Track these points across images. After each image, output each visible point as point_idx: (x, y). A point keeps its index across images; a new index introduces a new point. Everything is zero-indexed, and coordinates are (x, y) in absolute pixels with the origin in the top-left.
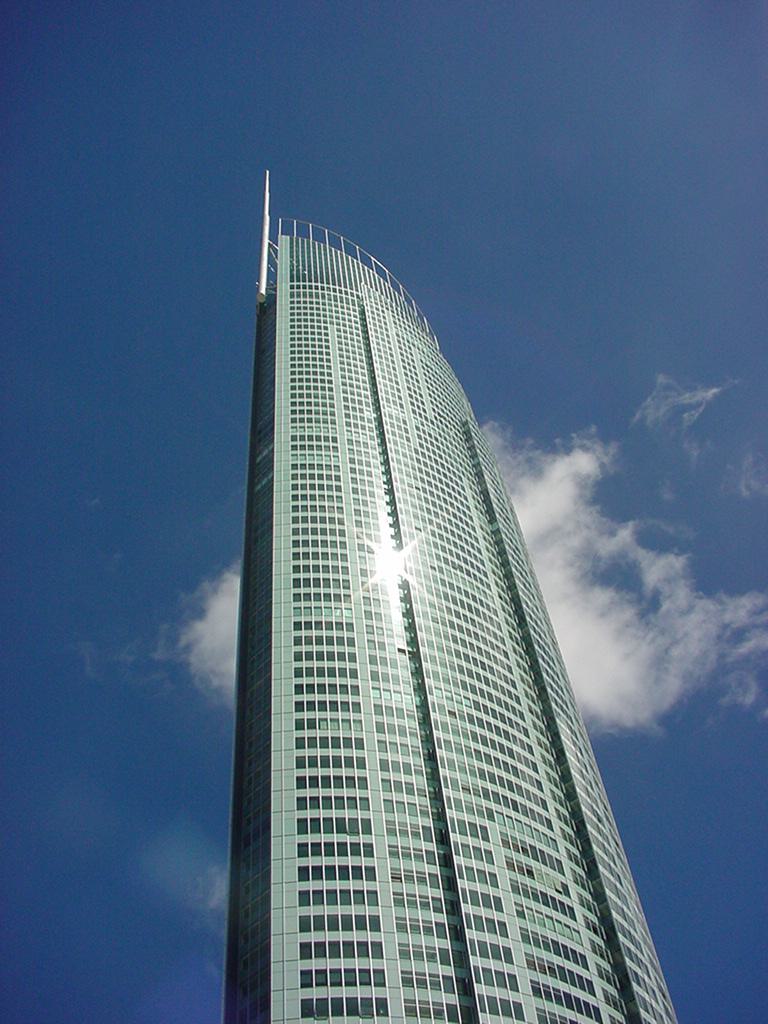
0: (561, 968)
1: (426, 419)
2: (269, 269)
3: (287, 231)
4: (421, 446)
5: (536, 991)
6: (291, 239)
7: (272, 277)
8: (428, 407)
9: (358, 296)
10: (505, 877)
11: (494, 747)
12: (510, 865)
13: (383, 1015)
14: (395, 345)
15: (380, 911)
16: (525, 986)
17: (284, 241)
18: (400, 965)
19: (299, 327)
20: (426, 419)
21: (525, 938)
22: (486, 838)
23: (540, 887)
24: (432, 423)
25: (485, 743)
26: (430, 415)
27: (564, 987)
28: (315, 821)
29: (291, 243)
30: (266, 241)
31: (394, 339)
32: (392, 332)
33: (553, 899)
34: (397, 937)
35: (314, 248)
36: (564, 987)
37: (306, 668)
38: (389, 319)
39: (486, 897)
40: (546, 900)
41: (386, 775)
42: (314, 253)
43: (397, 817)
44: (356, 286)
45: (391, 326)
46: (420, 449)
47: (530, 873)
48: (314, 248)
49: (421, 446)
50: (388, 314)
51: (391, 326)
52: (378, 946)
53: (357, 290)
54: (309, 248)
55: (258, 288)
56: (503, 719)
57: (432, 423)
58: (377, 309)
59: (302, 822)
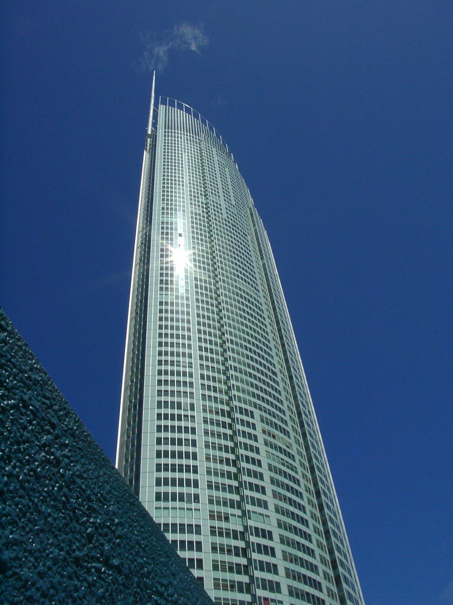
0: (287, 485)
1: (231, 204)
2: (154, 109)
3: (164, 103)
4: (228, 217)
5: (282, 541)
6: (166, 107)
7: (155, 125)
8: (232, 198)
9: (199, 139)
10: (261, 437)
11: (258, 372)
12: (264, 432)
13: (196, 502)
14: (217, 166)
15: (198, 477)
16: (271, 507)
17: (162, 108)
18: (205, 464)
19: (168, 183)
20: (231, 204)
21: (270, 469)
22: (253, 417)
23: (279, 444)
24: (234, 206)
25: (244, 332)
26: (233, 202)
27: (287, 481)
28: (166, 465)
29: (166, 109)
30: (151, 119)
31: (216, 162)
32: (216, 159)
33: (280, 427)
34: (210, 539)
35: (177, 113)
36: (287, 481)
37: (161, 500)
38: (215, 153)
39: (251, 446)
40: (281, 450)
41: (202, 362)
42: (177, 116)
43: (207, 403)
44: (198, 134)
45: (215, 156)
46: (227, 219)
47: (274, 437)
48: (177, 113)
49: (228, 217)
50: (214, 150)
51: (215, 156)
52: (199, 544)
53: (198, 136)
54: (174, 112)
55: (147, 131)
56: (255, 331)
57: (234, 206)
58: (209, 147)
59: (159, 403)
